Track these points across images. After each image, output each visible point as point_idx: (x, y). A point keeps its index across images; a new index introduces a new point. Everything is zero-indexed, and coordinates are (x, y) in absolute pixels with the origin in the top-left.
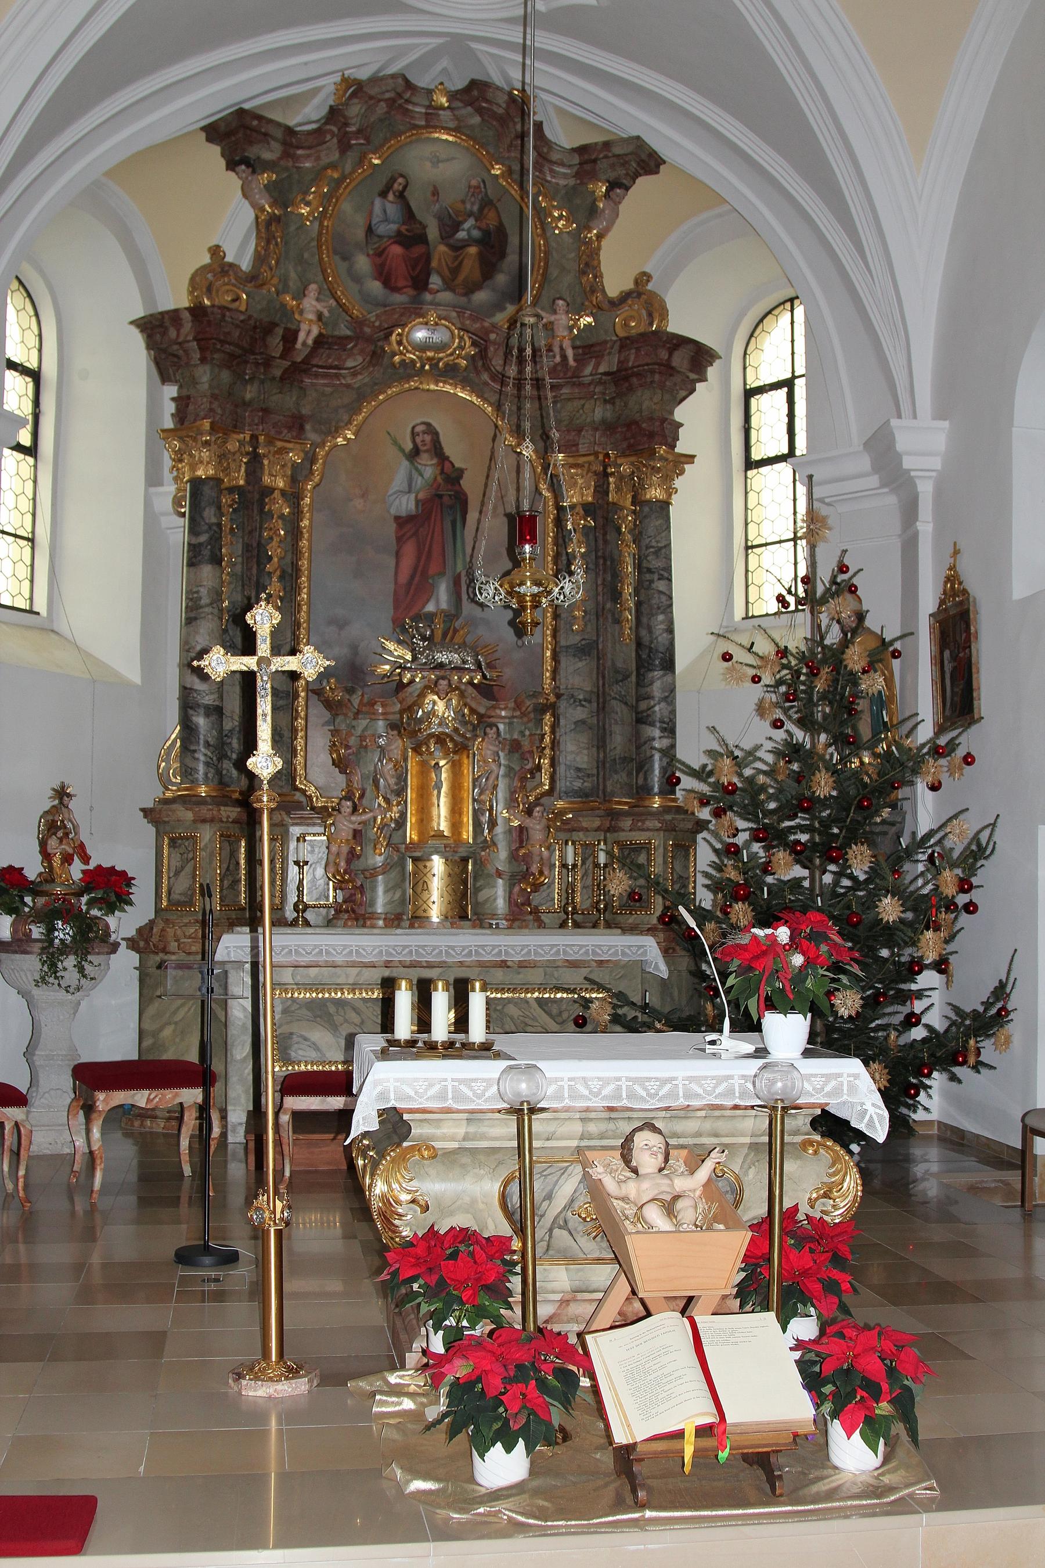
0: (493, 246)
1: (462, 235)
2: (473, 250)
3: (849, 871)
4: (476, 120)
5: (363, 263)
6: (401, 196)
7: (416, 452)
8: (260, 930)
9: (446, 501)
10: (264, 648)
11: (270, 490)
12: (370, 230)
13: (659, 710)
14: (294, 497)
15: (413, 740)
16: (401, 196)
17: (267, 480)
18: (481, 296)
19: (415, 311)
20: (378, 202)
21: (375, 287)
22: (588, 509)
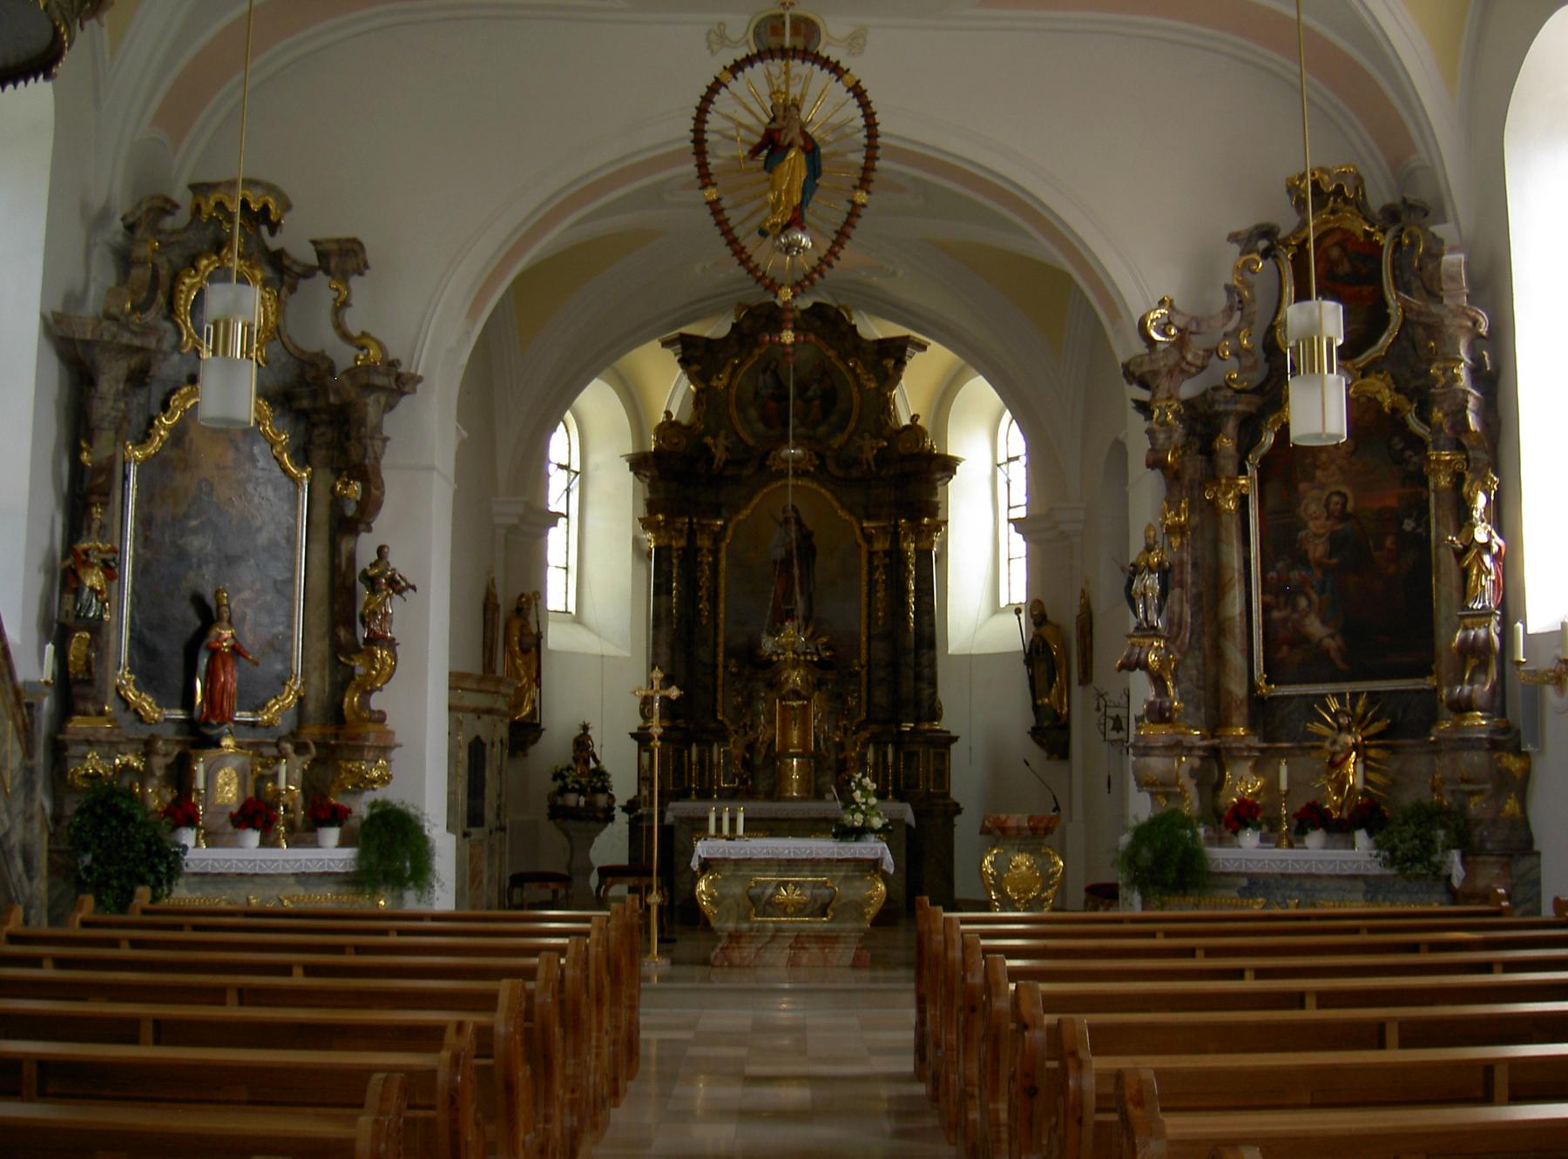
0: (829, 398)
1: (810, 393)
2: (817, 402)
3: (84, 445)
4: (819, 323)
5: (753, 413)
6: (774, 372)
7: (786, 521)
8: (694, 1051)
9: (806, 548)
10: (663, 693)
11: (700, 549)
12: (756, 394)
13: (926, 672)
14: (715, 552)
15: (1123, 892)
16: (774, 372)
17: (699, 543)
18: (822, 430)
19: (783, 440)
20: (761, 377)
21: (760, 427)
22: (887, 553)
